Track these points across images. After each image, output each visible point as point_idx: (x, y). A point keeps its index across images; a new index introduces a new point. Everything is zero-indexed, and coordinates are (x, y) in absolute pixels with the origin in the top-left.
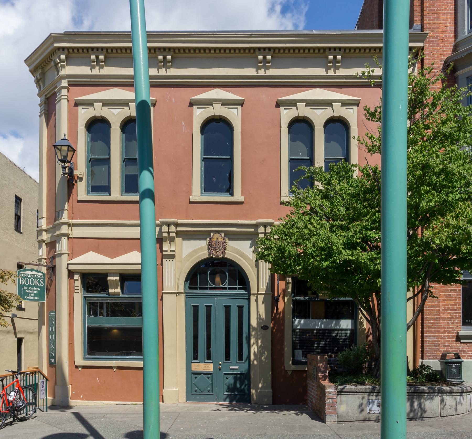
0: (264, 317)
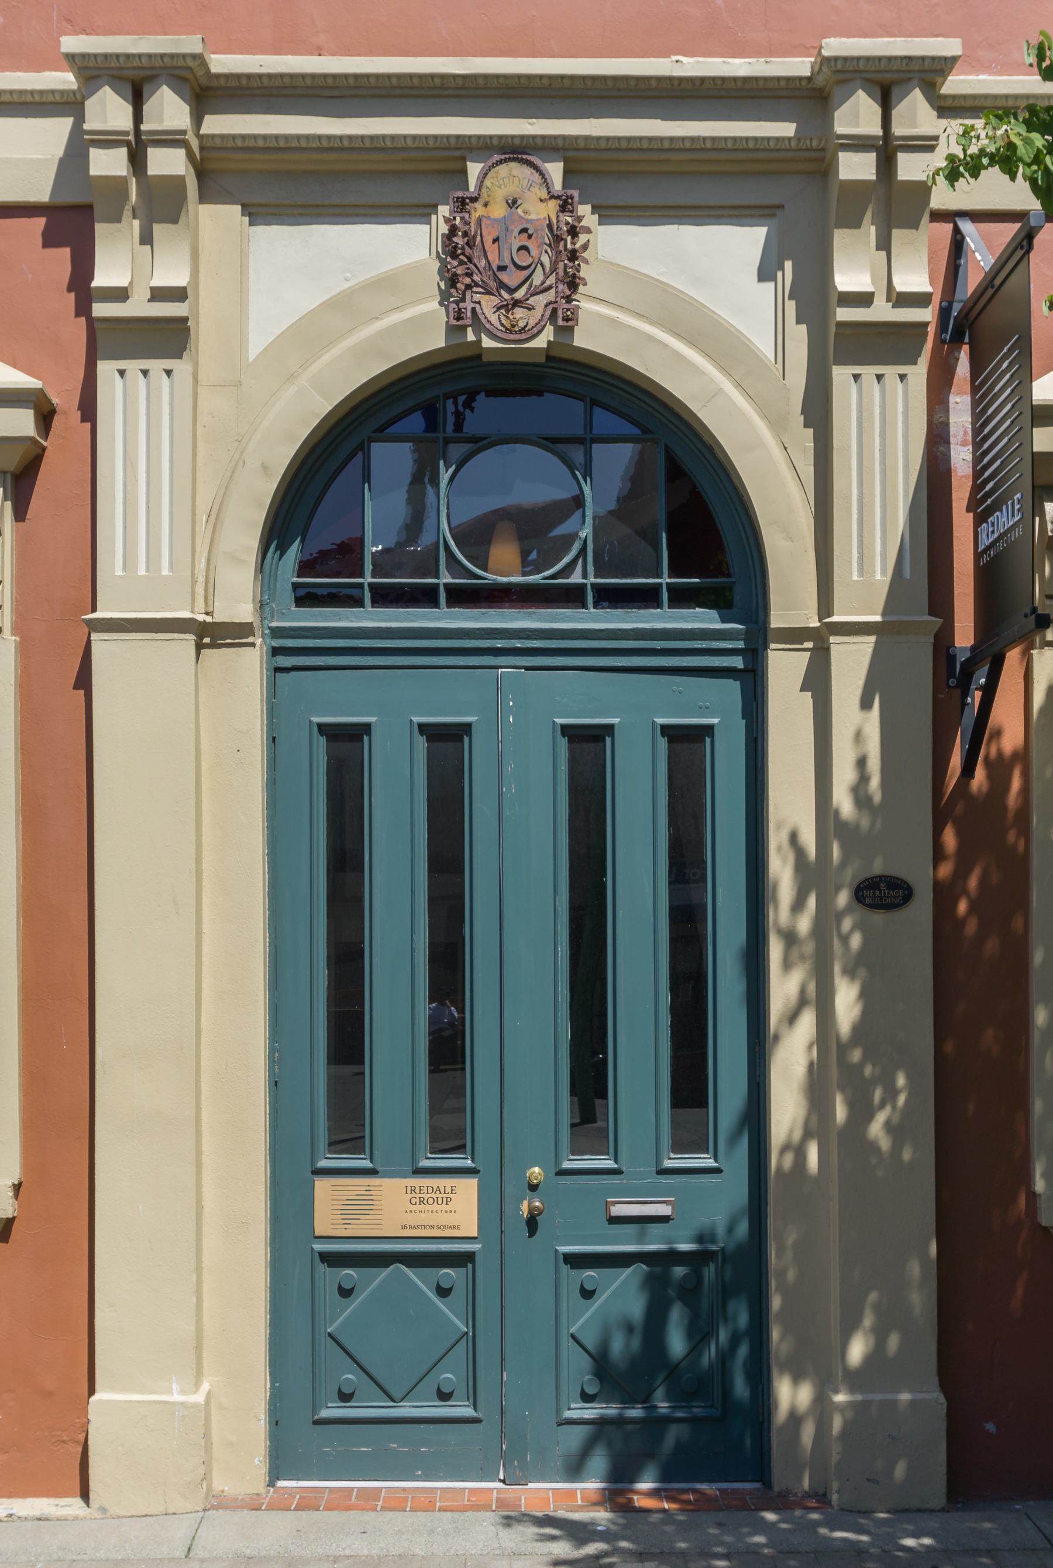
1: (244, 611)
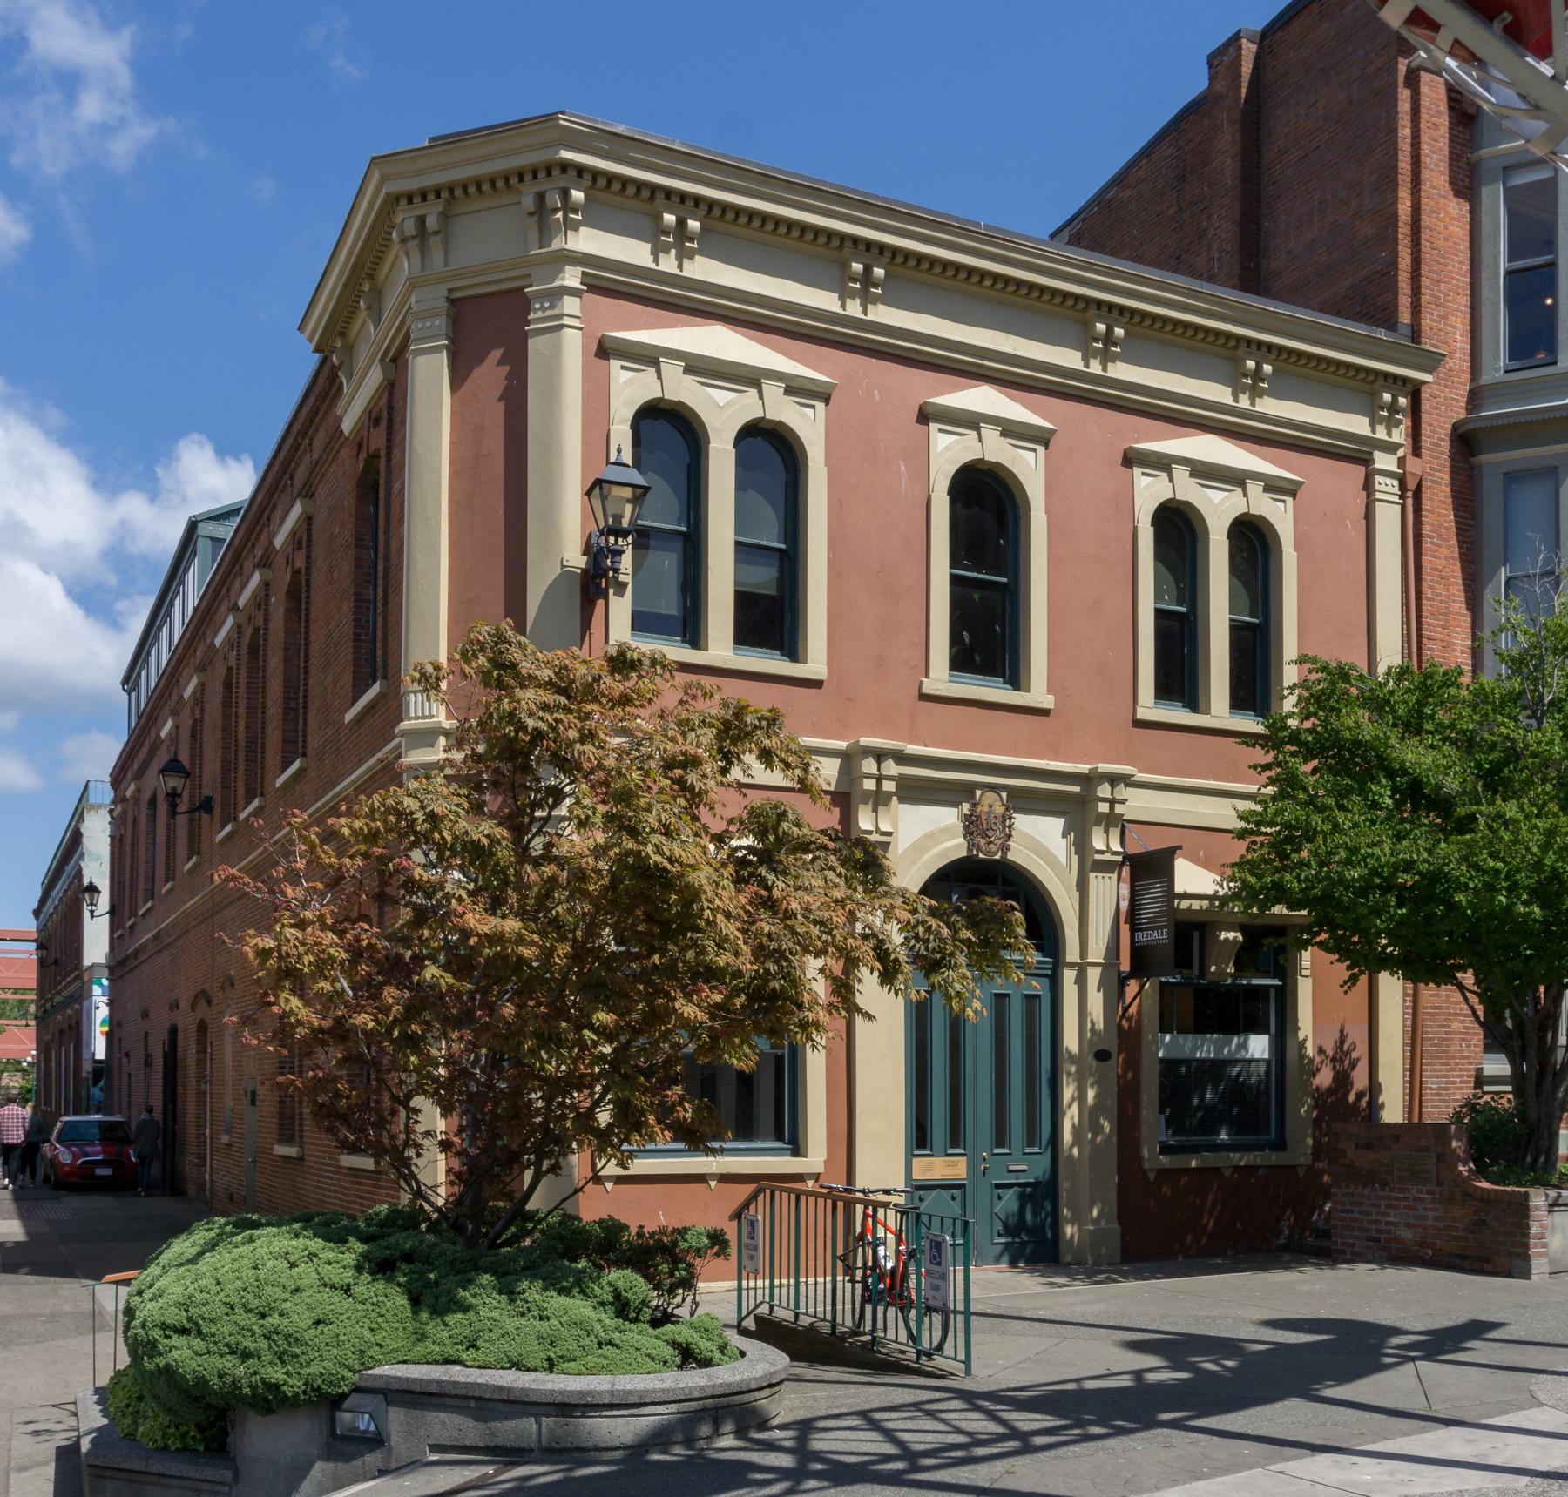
0: (1102, 1027)
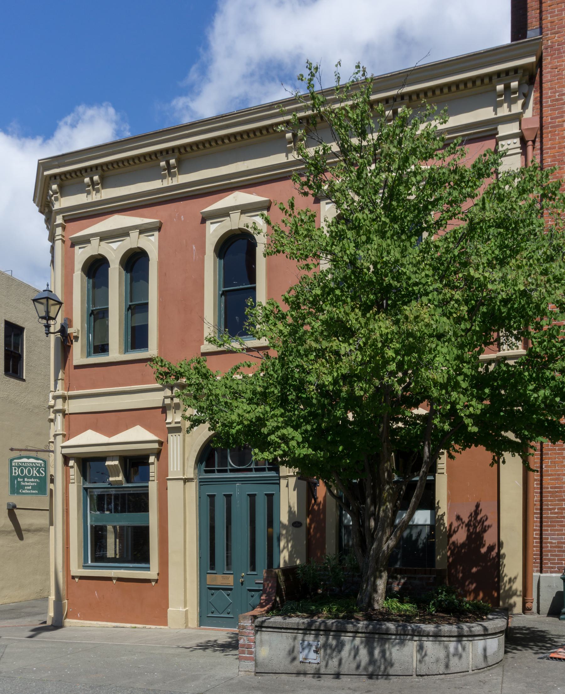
0: (296, 509)
1: (192, 476)
